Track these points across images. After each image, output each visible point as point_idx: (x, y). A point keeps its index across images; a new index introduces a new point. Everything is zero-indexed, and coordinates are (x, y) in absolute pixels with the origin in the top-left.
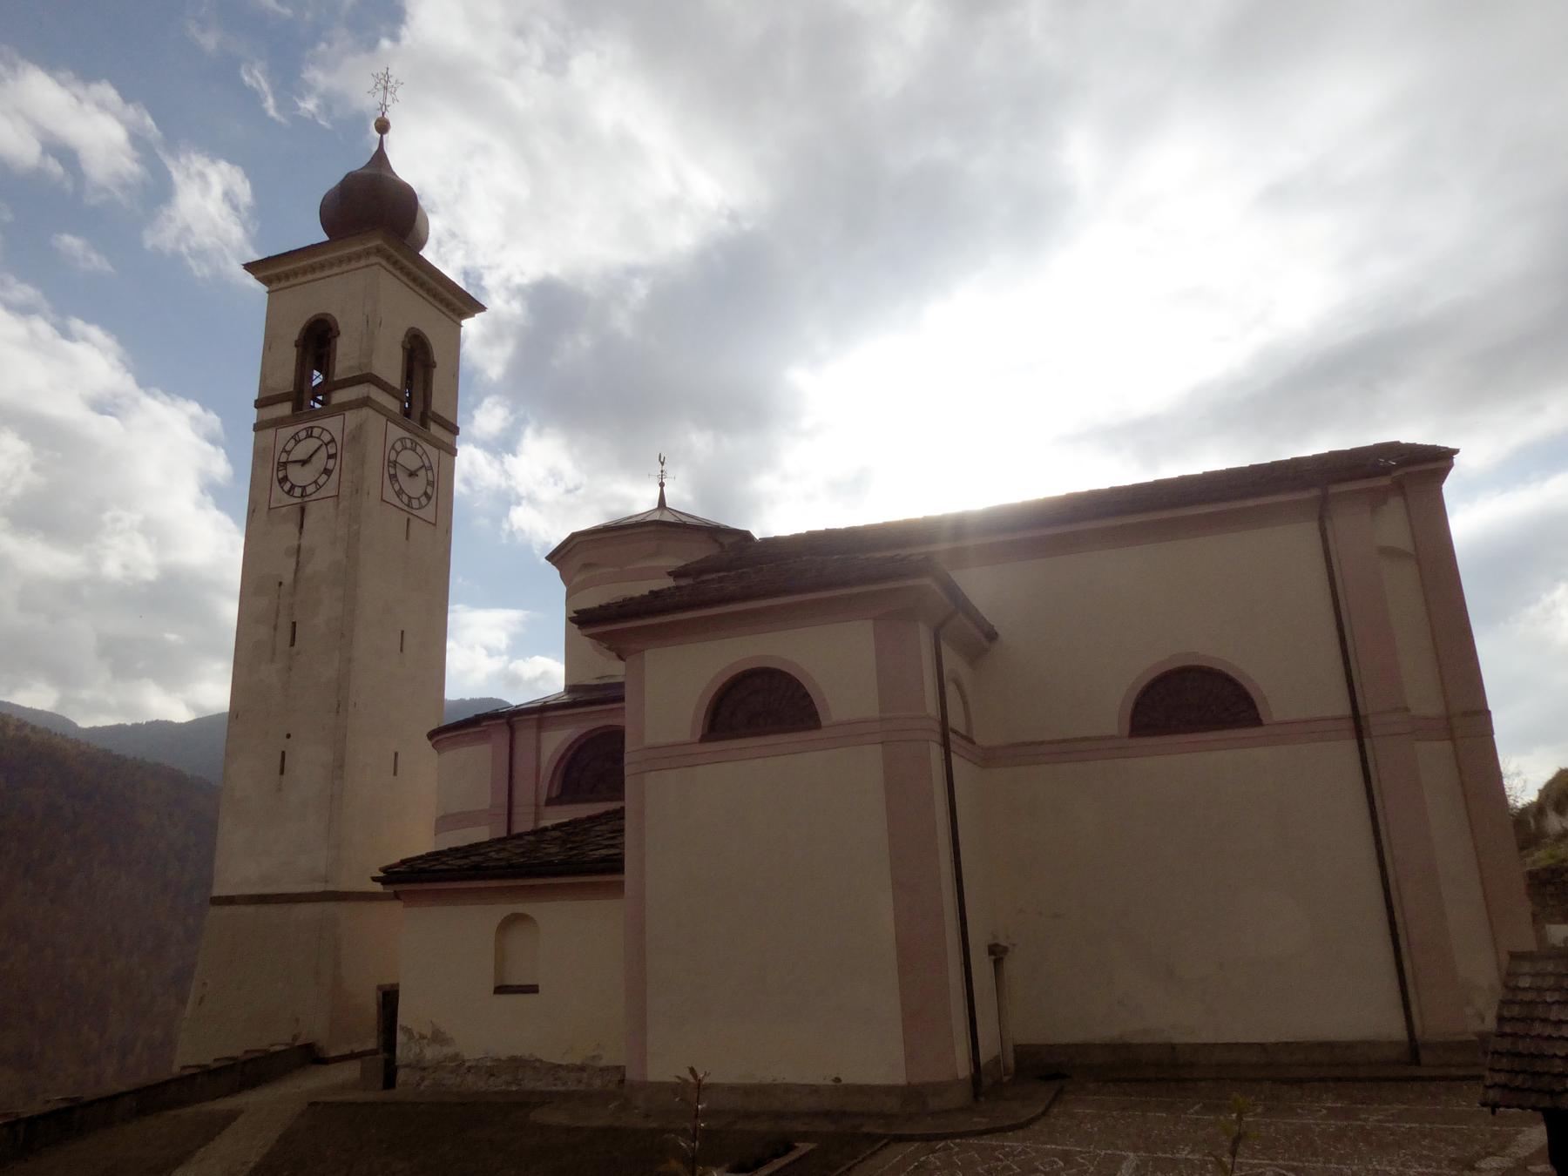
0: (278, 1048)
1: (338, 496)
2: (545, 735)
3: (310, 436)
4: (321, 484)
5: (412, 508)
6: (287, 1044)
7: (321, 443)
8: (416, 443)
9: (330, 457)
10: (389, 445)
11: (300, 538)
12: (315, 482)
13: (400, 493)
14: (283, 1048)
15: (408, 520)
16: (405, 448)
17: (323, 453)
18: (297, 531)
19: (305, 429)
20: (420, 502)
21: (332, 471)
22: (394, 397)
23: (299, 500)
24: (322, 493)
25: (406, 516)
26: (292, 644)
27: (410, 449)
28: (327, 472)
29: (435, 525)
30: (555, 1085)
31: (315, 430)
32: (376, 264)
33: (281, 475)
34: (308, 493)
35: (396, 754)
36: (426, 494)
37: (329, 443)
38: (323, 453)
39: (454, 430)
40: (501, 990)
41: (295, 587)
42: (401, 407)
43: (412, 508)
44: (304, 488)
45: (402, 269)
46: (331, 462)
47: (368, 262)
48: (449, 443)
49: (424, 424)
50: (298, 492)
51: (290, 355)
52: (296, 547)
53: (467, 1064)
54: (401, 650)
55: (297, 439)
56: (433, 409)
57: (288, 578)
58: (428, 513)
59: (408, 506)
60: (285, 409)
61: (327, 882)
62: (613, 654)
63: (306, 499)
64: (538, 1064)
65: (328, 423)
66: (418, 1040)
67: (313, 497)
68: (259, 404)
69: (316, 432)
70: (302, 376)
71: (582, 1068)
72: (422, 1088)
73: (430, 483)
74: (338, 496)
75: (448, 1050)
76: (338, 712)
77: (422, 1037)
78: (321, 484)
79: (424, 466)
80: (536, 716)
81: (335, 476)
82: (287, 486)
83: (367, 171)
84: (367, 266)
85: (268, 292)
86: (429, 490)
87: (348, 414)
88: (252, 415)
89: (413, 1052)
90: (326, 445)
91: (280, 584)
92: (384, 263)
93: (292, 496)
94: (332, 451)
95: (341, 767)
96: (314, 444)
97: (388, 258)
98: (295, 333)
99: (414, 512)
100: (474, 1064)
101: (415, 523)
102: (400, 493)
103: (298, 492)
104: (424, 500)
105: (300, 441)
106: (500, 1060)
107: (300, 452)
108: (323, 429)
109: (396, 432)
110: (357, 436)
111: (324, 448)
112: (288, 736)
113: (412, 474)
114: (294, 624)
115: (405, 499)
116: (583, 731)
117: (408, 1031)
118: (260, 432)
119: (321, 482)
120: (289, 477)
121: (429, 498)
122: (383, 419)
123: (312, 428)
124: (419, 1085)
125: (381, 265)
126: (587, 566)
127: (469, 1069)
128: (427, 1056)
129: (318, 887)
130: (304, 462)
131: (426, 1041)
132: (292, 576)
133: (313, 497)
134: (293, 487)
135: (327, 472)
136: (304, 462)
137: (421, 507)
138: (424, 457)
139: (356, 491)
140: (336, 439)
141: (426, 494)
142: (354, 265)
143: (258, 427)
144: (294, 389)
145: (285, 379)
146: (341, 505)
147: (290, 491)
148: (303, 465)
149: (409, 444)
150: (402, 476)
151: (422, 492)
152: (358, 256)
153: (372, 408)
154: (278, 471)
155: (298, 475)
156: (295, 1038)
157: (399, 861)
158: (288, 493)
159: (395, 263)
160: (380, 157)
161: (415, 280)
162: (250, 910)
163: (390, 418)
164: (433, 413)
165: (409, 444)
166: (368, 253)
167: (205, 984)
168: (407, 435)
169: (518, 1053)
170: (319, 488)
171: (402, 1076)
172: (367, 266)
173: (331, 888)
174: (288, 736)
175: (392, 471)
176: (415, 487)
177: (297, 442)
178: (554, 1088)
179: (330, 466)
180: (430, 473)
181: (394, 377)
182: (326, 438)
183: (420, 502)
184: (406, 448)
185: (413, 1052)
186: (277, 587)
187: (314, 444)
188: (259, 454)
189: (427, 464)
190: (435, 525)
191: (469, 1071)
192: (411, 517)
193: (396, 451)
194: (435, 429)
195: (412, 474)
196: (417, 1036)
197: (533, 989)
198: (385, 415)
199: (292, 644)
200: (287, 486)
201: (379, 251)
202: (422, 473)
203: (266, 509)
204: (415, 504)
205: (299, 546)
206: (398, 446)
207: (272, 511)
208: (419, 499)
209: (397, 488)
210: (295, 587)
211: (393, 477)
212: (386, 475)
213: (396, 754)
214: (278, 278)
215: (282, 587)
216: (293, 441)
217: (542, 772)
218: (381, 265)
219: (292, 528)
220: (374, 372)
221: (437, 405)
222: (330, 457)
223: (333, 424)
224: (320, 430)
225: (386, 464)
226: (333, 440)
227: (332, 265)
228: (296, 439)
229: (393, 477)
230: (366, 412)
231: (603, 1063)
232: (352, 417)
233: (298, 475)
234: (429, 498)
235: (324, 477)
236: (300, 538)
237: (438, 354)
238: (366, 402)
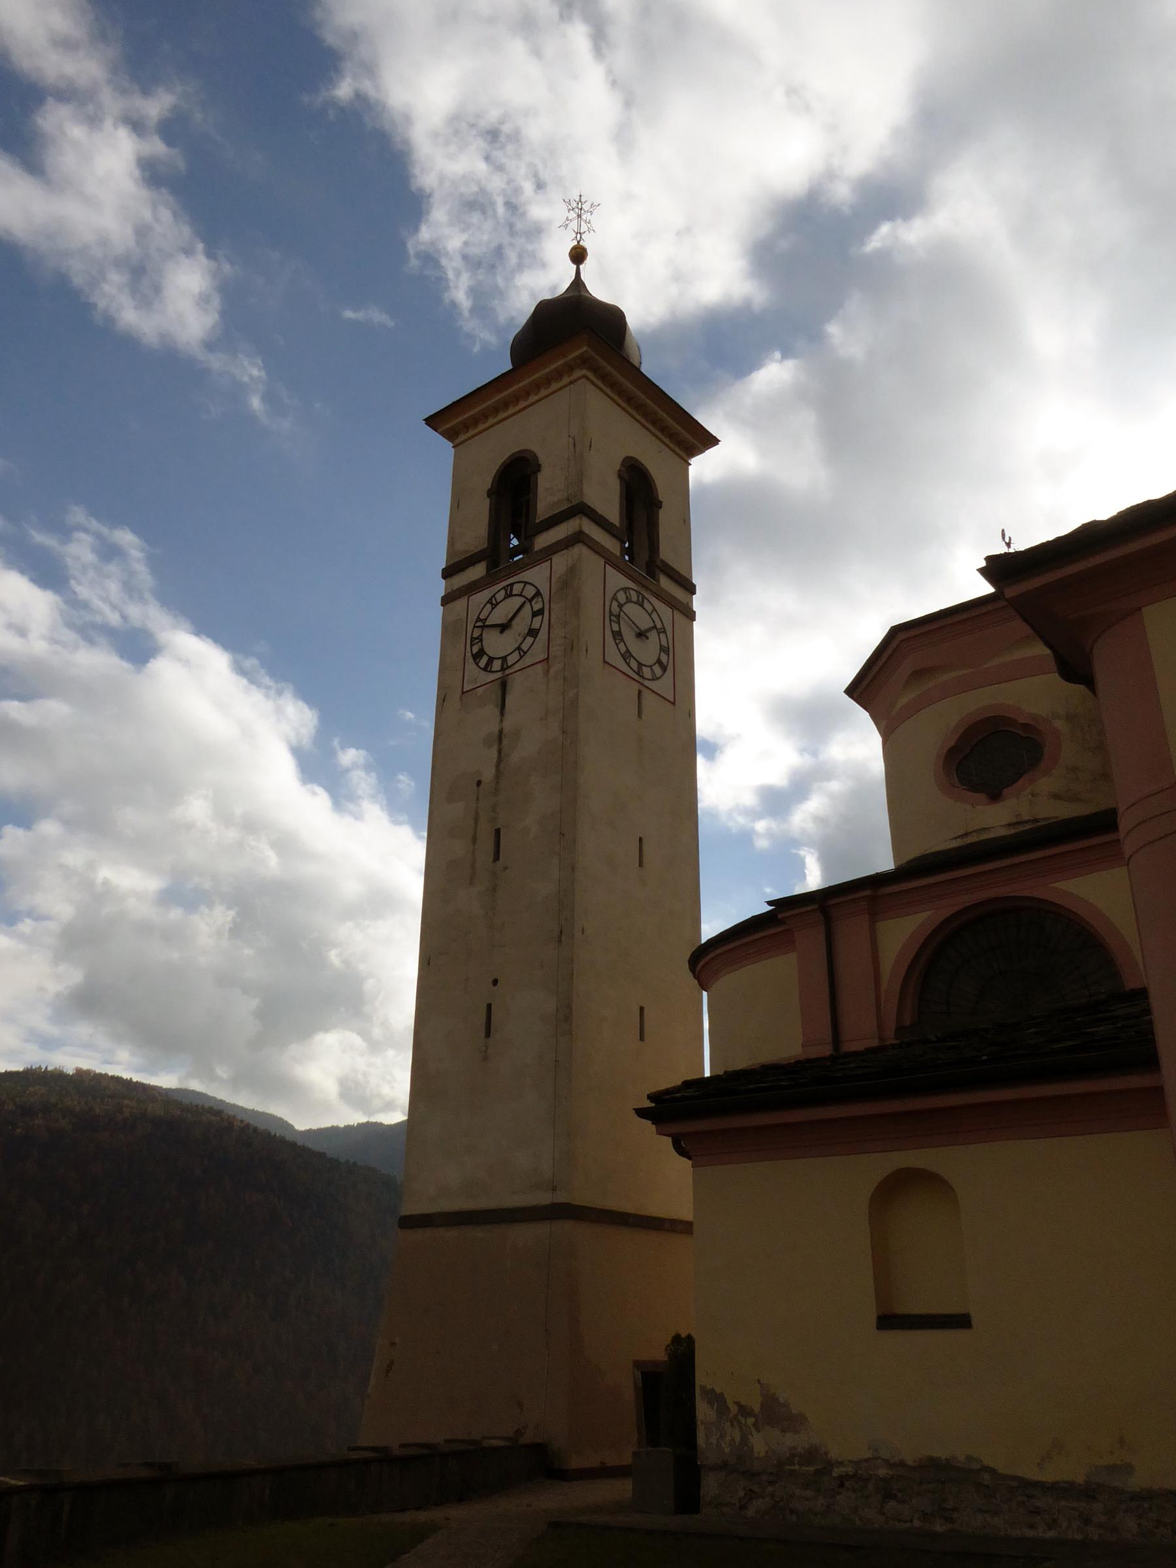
0: (494, 1443)
1: (548, 659)
2: (882, 926)
3: (509, 595)
4: (525, 650)
5: (642, 677)
6: (506, 1439)
7: (523, 600)
8: (644, 597)
9: (535, 614)
10: (609, 597)
11: (501, 721)
12: (519, 648)
13: (627, 656)
14: (501, 1443)
15: (640, 692)
16: (629, 600)
17: (527, 611)
18: (497, 712)
19: (504, 588)
20: (652, 671)
21: (539, 630)
22: (614, 536)
23: (499, 675)
24: (527, 660)
25: (636, 686)
26: (496, 857)
27: (635, 603)
28: (533, 633)
29: (674, 703)
30: (1032, 1526)
31: (515, 586)
32: (580, 378)
33: (476, 649)
34: (509, 664)
35: (642, 1009)
36: (659, 662)
37: (533, 598)
38: (527, 611)
39: (691, 589)
40: (888, 1321)
41: (497, 783)
42: (621, 548)
43: (642, 677)
44: (504, 659)
45: (613, 385)
46: (538, 619)
47: (572, 378)
48: (685, 602)
49: (652, 575)
50: (497, 665)
51: (481, 508)
52: (497, 731)
53: (836, 1472)
54: (641, 865)
55: (494, 602)
56: (661, 557)
57: (488, 775)
58: (663, 686)
59: (638, 674)
60: (478, 571)
61: (554, 1189)
62: (982, 797)
63: (507, 672)
64: (986, 1478)
65: (531, 575)
66: (736, 1416)
67: (517, 667)
68: (447, 573)
69: (517, 589)
70: (496, 536)
71: (1088, 1492)
72: (750, 1513)
73: (664, 650)
74: (548, 659)
75: (790, 1440)
76: (560, 941)
77: (744, 1410)
78: (525, 650)
79: (655, 627)
80: (867, 893)
81: (543, 635)
82: (483, 661)
83: (565, 296)
84: (571, 383)
85: (453, 447)
86: (664, 658)
87: (556, 559)
88: (440, 587)
89: (728, 1439)
90: (530, 601)
91: (479, 783)
92: (590, 375)
93: (490, 671)
94: (537, 607)
95: (568, 1018)
96: (516, 602)
97: (596, 370)
98: (486, 481)
99: (646, 683)
100: (850, 1470)
101: (648, 697)
102: (627, 656)
103: (497, 665)
104: (658, 670)
105: (498, 604)
106: (902, 1464)
107: (499, 616)
108: (526, 583)
109: (617, 580)
110: (568, 583)
111: (528, 606)
112: (495, 982)
113: (641, 635)
114: (498, 832)
115: (634, 665)
116: (946, 913)
117: (715, 1398)
118: (447, 606)
119: (525, 647)
120: (486, 650)
121: (664, 669)
122: (602, 561)
123: (512, 585)
124: (743, 1507)
125: (588, 379)
126: (919, 674)
127: (842, 1481)
128: (756, 1450)
129: (544, 1198)
130: (504, 627)
131: (751, 1420)
132: (493, 771)
133: (517, 667)
134: (491, 660)
135: (533, 633)
136: (504, 627)
137: (655, 678)
138: (654, 616)
139: (571, 647)
140: (542, 591)
141: (659, 662)
142: (555, 386)
143: (446, 600)
144: (488, 544)
145: (477, 535)
146: (552, 671)
147: (487, 665)
148: (502, 632)
149: (634, 597)
150: (628, 635)
151: (656, 659)
152: (559, 374)
153: (585, 544)
154: (472, 646)
155: (497, 645)
156: (519, 1433)
157: (679, 1083)
158: (485, 669)
159: (604, 377)
160: (578, 283)
161: (629, 400)
162: (449, 1234)
163: (609, 559)
164: (662, 561)
165: (634, 597)
166: (569, 368)
167: (393, 1344)
168: (630, 584)
169: (941, 1453)
170: (523, 653)
171: (710, 1486)
172: (571, 383)
173: (561, 1197)
174: (495, 982)
175: (615, 627)
176: (647, 652)
177: (494, 606)
178: (1030, 1533)
179: (536, 625)
180: (662, 636)
181: (613, 512)
182: (530, 592)
183: (652, 671)
184: (631, 601)
185: (728, 1439)
186: (475, 785)
187: (516, 602)
188: (449, 630)
189: (659, 626)
190: (674, 703)
191: (842, 1485)
192: (643, 689)
193: (617, 601)
194: (665, 583)
195: (641, 635)
196: (734, 1409)
197: (962, 1322)
198: (603, 557)
199: (496, 857)
200: (483, 661)
201: (583, 361)
202: (653, 635)
203: (460, 692)
204: (647, 672)
205: (501, 732)
206: (622, 597)
207: (466, 694)
208: (651, 667)
209: (623, 649)
210: (497, 783)
211: (618, 635)
212: (608, 634)
213: (642, 1009)
214: (466, 426)
215: (482, 786)
216: (489, 606)
217: (884, 985)
218: (588, 379)
219: (491, 710)
220: (585, 501)
221: (666, 553)
222: (535, 614)
223: (538, 576)
224: (523, 585)
225: (607, 618)
226: (538, 594)
227: (527, 394)
228: (493, 603)
229: (618, 635)
230: (579, 550)
231: (1138, 1481)
232: (560, 562)
233: (497, 645)
234: (664, 669)
235: (530, 640)
236: (501, 721)
237: (663, 492)
238: (578, 538)
